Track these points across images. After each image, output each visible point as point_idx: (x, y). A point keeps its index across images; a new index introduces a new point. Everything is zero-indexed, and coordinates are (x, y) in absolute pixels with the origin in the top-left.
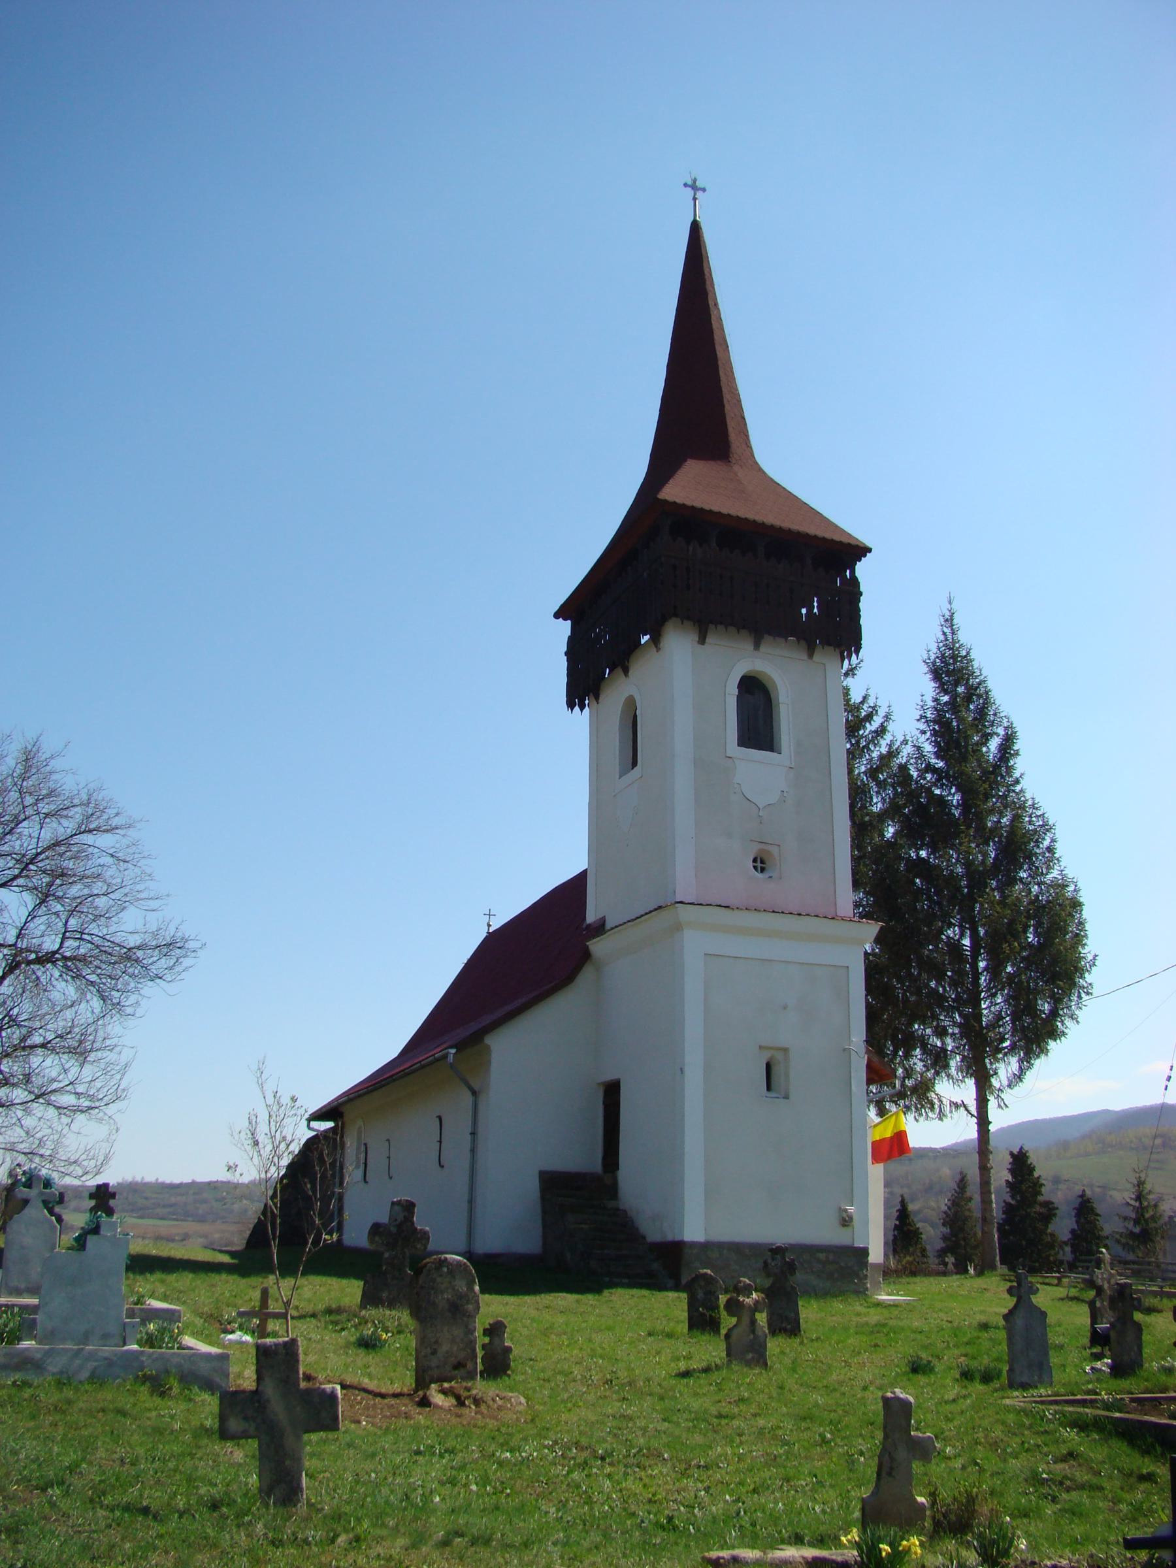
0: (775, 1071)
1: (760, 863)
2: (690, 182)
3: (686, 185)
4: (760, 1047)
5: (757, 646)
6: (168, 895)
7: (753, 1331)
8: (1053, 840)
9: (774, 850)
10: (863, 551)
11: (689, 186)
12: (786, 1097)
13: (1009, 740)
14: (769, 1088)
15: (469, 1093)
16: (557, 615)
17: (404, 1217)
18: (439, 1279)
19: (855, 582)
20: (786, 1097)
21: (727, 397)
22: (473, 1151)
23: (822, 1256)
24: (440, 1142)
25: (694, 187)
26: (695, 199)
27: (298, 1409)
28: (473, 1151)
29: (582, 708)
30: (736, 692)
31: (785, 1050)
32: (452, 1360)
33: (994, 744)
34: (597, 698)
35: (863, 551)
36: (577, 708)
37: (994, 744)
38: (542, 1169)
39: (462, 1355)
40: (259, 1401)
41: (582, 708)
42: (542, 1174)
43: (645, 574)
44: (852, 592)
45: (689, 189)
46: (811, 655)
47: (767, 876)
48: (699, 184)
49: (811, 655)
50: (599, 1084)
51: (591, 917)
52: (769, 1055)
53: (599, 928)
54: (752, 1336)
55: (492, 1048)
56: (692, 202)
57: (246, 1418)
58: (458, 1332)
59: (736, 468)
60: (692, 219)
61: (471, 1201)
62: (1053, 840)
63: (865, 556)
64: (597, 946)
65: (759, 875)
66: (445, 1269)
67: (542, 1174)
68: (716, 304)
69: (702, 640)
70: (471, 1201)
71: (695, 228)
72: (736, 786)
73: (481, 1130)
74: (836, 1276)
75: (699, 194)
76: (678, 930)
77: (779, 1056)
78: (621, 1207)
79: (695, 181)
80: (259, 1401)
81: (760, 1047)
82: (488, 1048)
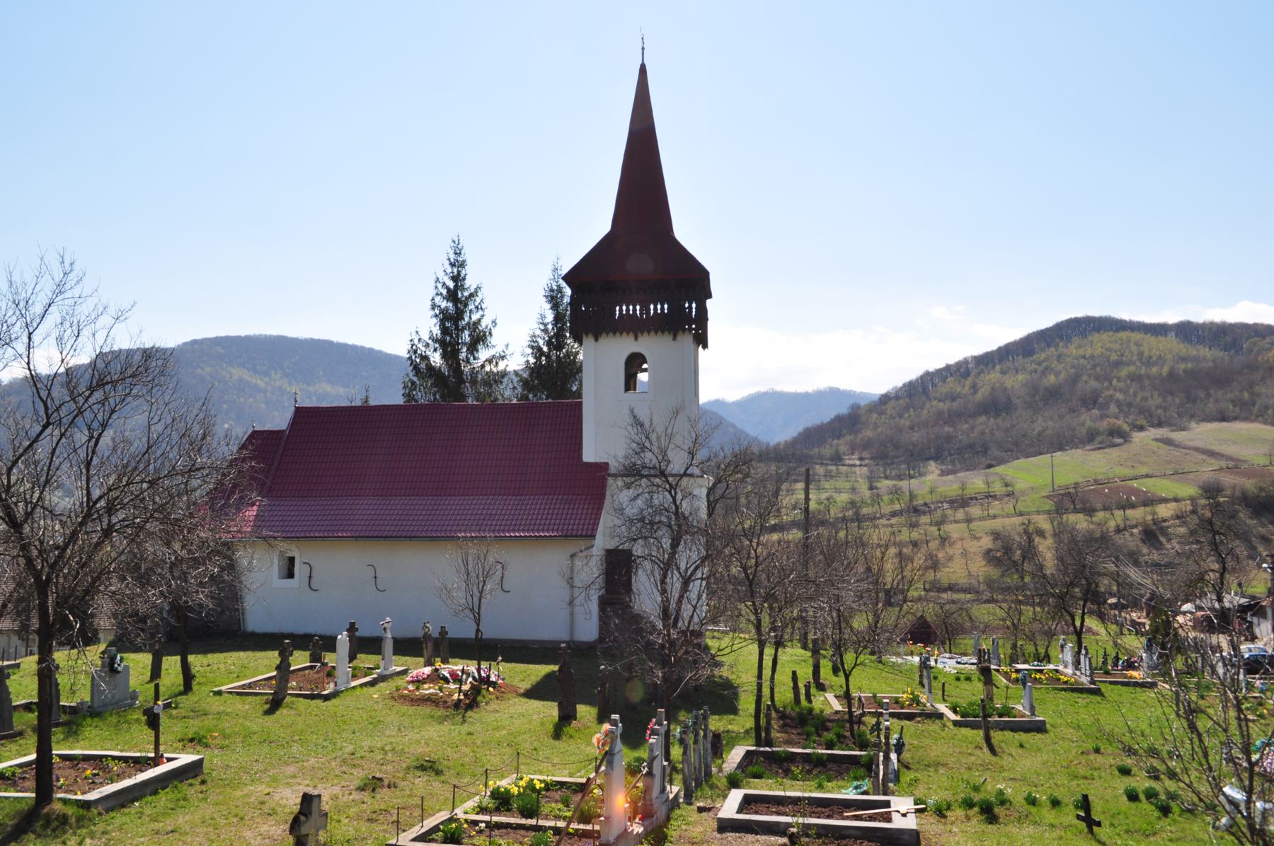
71: (643, 70)
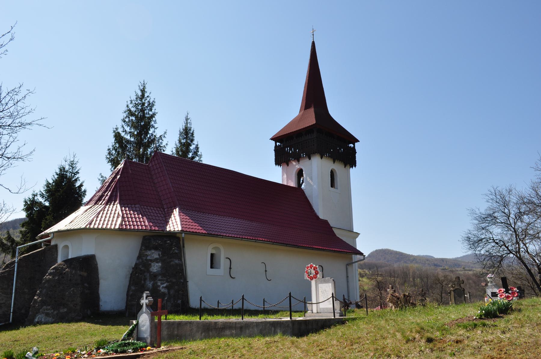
35: (357, 141)
63: (357, 142)
71: (313, 44)
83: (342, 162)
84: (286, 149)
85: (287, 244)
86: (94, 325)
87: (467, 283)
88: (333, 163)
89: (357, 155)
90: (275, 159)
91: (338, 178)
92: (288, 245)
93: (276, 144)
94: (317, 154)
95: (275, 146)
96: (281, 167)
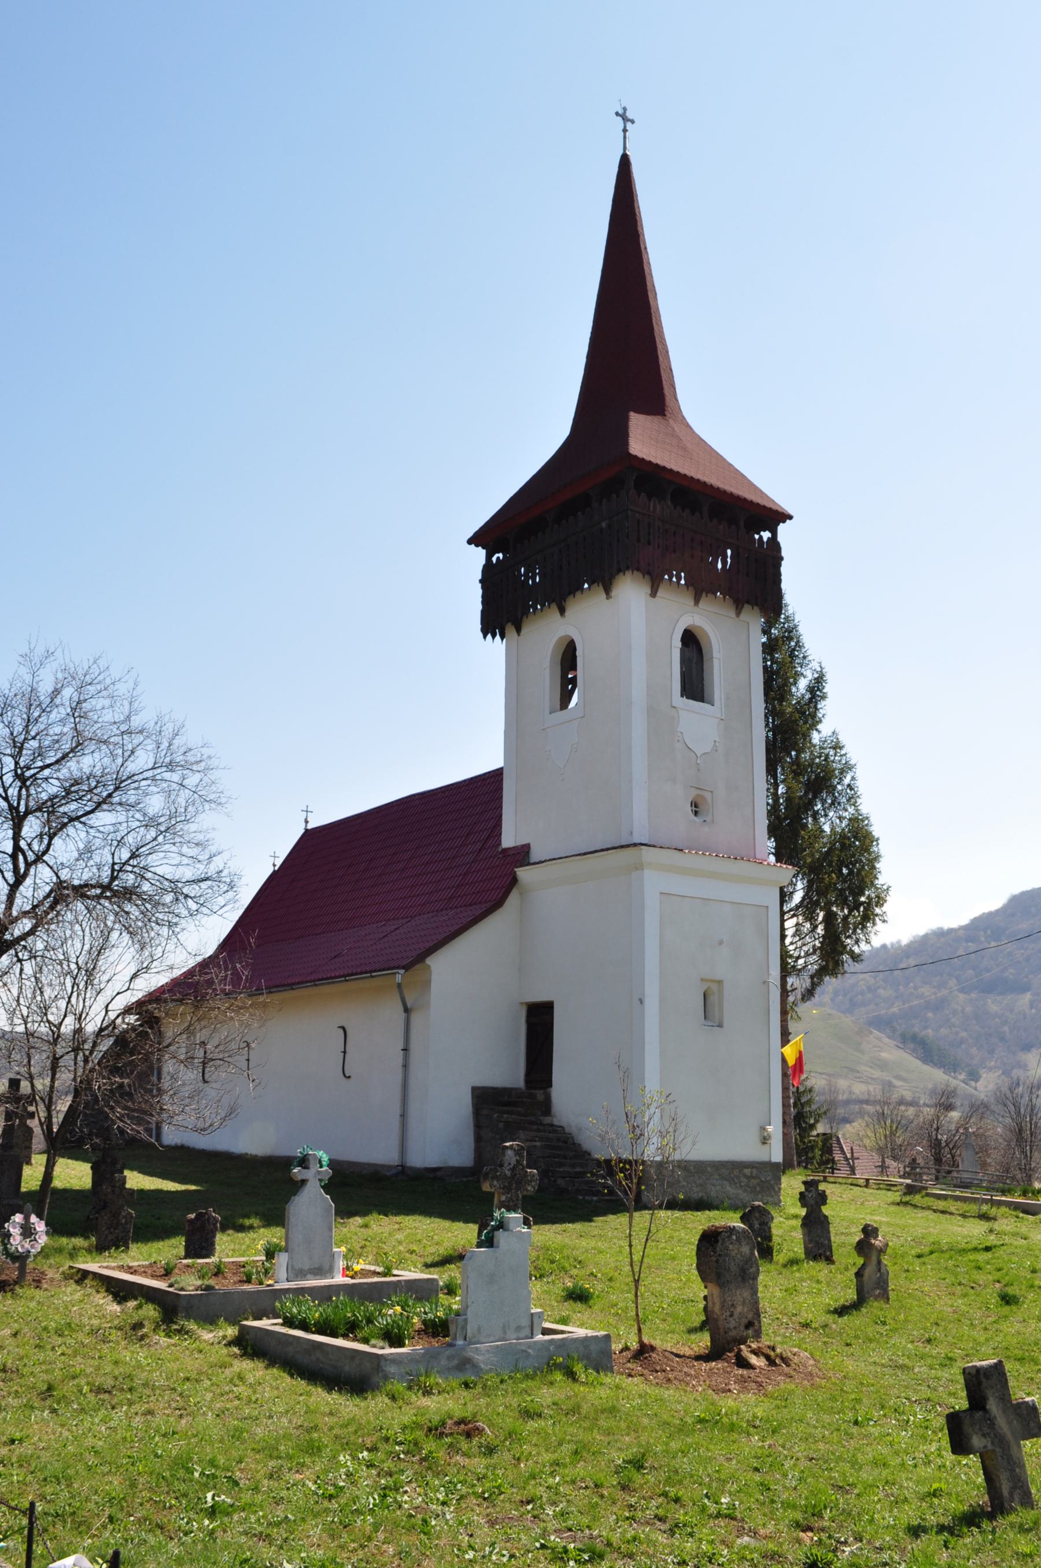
0: (713, 999)
1: (696, 807)
2: (621, 112)
3: (617, 114)
4: (702, 980)
5: (697, 602)
6: (214, 829)
7: (879, 1270)
8: (853, 778)
9: (707, 795)
10: (785, 517)
11: (620, 116)
12: (720, 1026)
13: (820, 680)
14: (705, 1018)
15: (402, 1009)
16: (470, 542)
17: (517, 1160)
18: (731, 1247)
19: (774, 544)
20: (720, 1026)
21: (659, 346)
22: (405, 1066)
23: (747, 1171)
24: (345, 1052)
25: (625, 119)
26: (625, 130)
27: (1015, 1422)
28: (405, 1066)
29: (494, 637)
30: (680, 645)
31: (720, 983)
32: (745, 1321)
33: (803, 684)
34: (519, 630)
35: (785, 517)
36: (489, 636)
37: (803, 684)
38: (478, 1083)
39: (750, 1316)
40: (989, 1419)
41: (494, 637)
42: (474, 1089)
43: (604, 525)
44: (773, 555)
45: (620, 119)
46: (738, 614)
47: (702, 820)
48: (629, 115)
49: (738, 614)
50: (521, 1003)
51: (509, 840)
52: (706, 987)
53: (522, 855)
54: (878, 1275)
55: (432, 969)
56: (622, 133)
57: (984, 1435)
58: (746, 1294)
59: (671, 421)
60: (621, 152)
61: (403, 1116)
62: (853, 778)
63: (784, 522)
64: (523, 873)
65: (695, 818)
66: (734, 1237)
67: (474, 1089)
68: (646, 248)
69: (654, 594)
70: (403, 1116)
71: (625, 163)
72: (679, 734)
73: (414, 1046)
74: (758, 1189)
75: (629, 125)
76: (637, 869)
77: (714, 987)
78: (556, 1123)
79: (625, 109)
80: (989, 1419)
81: (702, 980)
82: (429, 967)
83: (756, 608)
84: (538, 580)
85: (294, 984)
86: (447, 1224)
87: (446, 1446)
88: (693, 603)
89: (784, 569)
90: (482, 611)
91: (716, 662)
92: (375, 971)
93: (489, 557)
94: (628, 573)
95: (484, 566)
96: (504, 640)
